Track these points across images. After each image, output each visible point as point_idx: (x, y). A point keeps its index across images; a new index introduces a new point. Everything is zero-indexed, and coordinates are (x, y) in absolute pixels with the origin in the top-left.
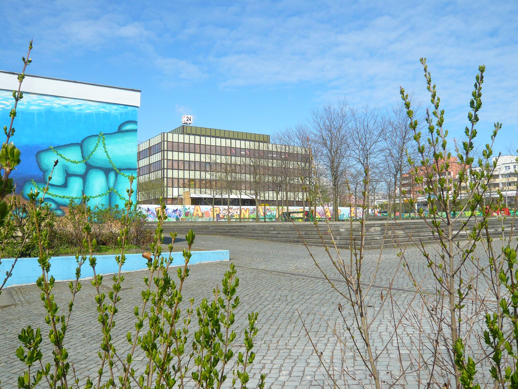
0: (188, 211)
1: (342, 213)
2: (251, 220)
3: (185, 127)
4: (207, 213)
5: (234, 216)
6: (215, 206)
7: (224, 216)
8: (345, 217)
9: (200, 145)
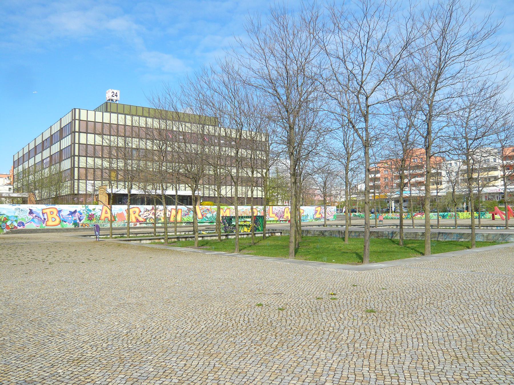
0: (93, 213)
1: (305, 214)
2: (184, 224)
3: (109, 104)
4: (121, 215)
5: (160, 219)
6: (131, 206)
7: (146, 220)
8: (309, 218)
9: (125, 125)
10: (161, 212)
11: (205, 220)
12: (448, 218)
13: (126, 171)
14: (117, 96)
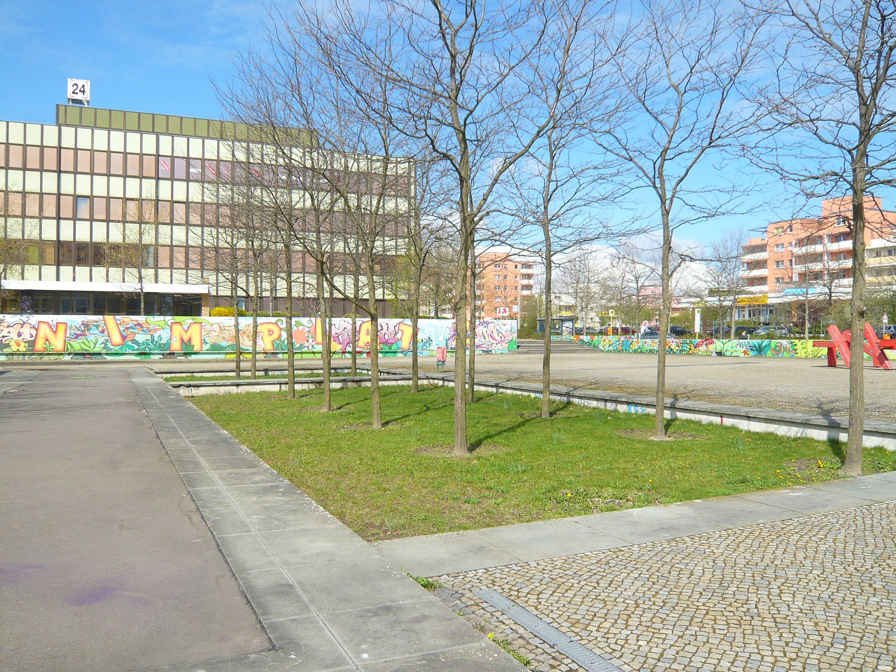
2: (67, 358)
5: (8, 346)
8: (434, 347)
10: (11, 329)
11: (130, 347)
12: (769, 353)
13: (59, 244)
14: (84, 92)
